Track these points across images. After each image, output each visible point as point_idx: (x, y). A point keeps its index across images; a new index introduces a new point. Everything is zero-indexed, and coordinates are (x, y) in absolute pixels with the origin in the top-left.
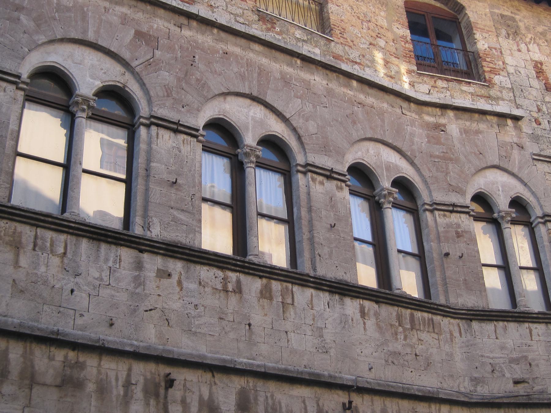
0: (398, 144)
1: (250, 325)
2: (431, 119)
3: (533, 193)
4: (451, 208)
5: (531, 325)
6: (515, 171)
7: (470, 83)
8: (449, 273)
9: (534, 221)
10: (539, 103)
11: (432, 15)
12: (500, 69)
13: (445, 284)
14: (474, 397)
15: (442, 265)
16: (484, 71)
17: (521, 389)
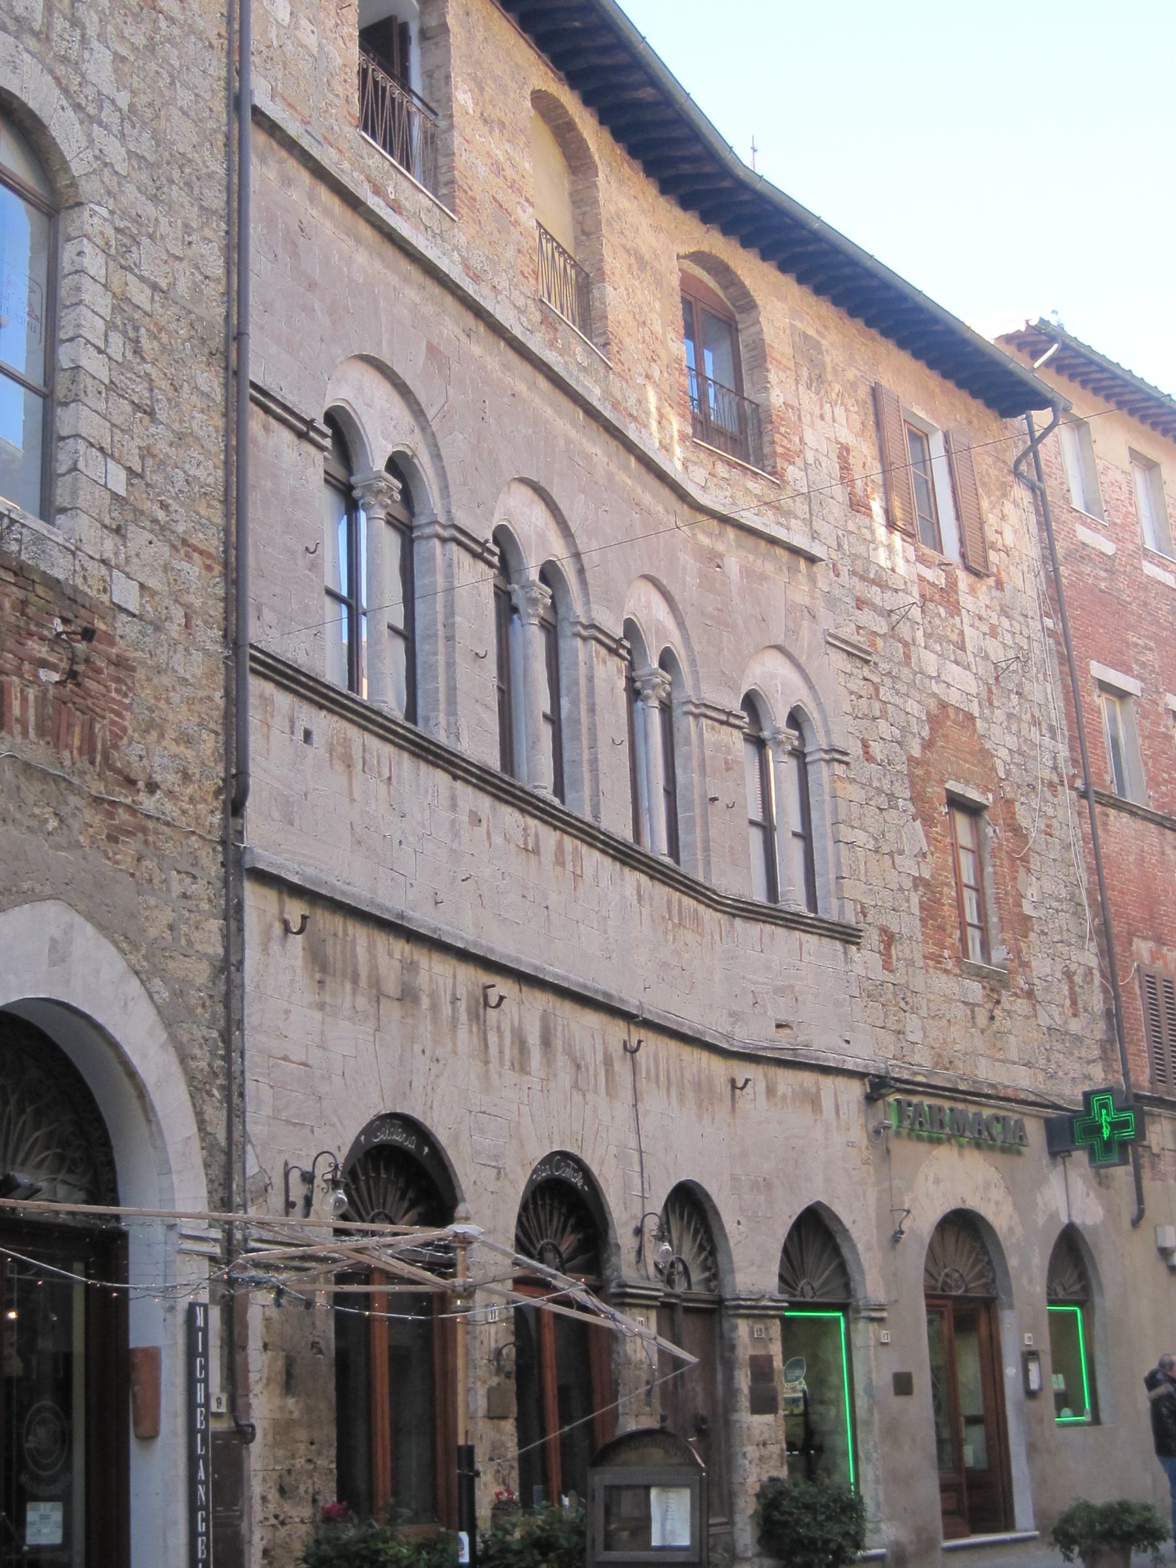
0: (672, 588)
1: (547, 908)
2: (705, 540)
3: (819, 704)
4: (723, 718)
5: (802, 934)
6: (803, 660)
7: (757, 474)
8: (713, 832)
9: (810, 753)
10: (840, 533)
11: (703, 305)
12: (795, 452)
13: (707, 849)
14: (735, 1043)
15: (705, 816)
16: (775, 453)
17: (783, 1039)
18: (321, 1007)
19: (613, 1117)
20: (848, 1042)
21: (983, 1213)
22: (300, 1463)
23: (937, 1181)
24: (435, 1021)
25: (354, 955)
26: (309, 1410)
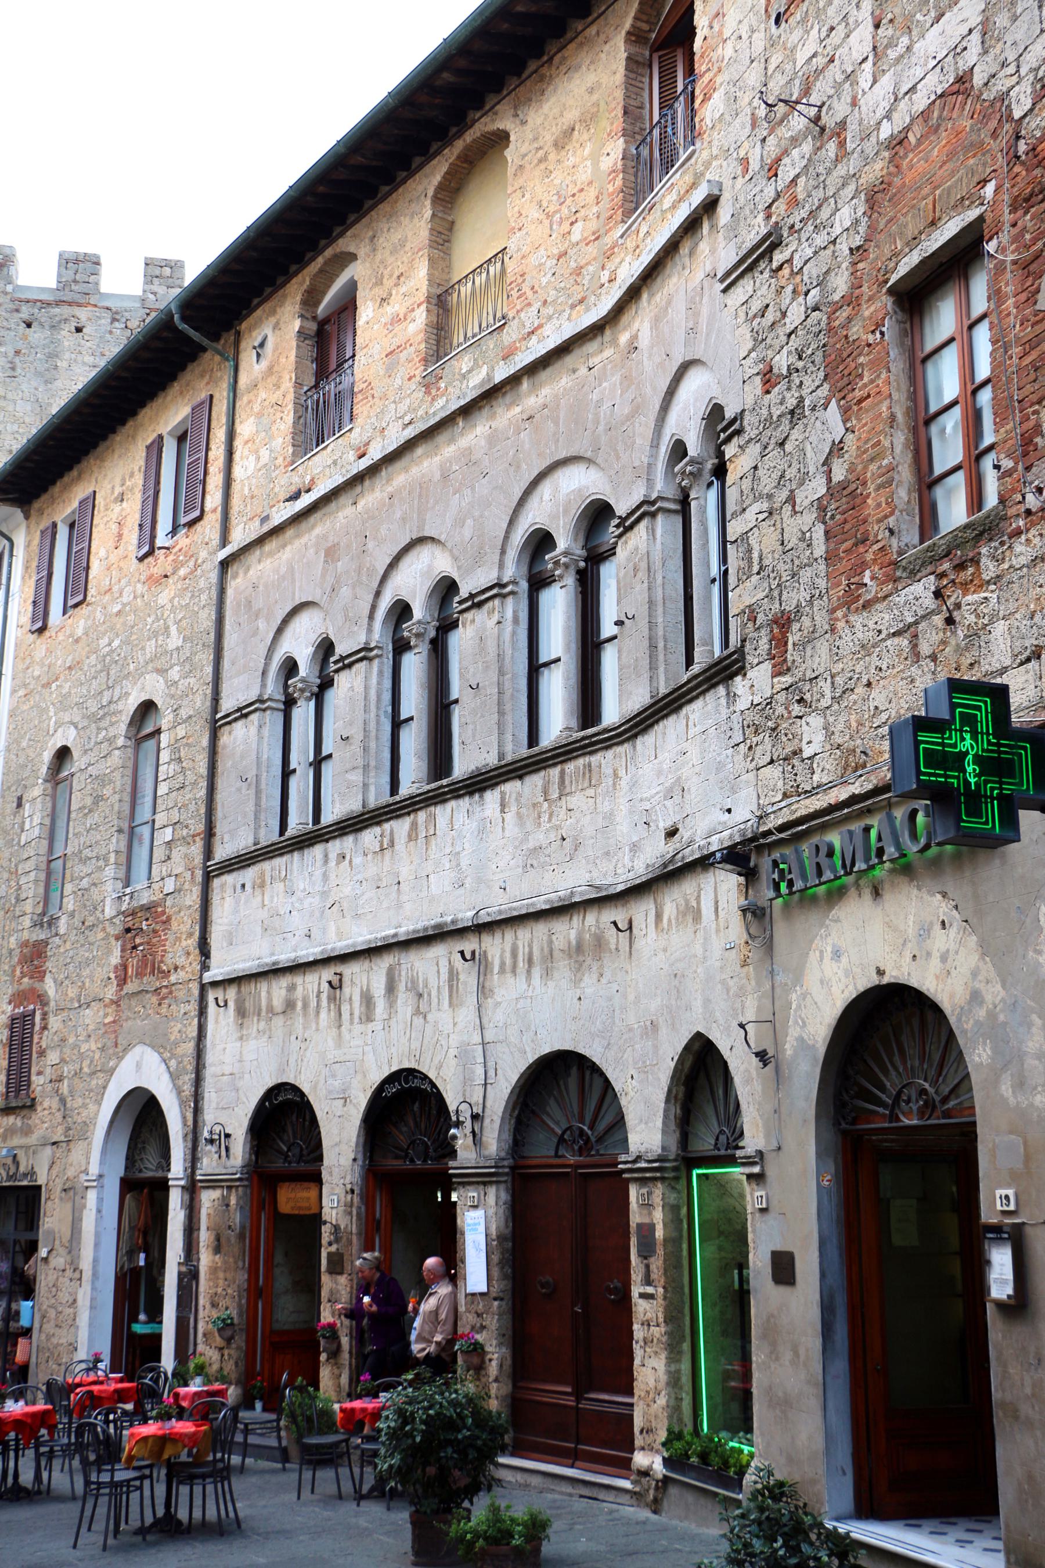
18: (241, 1038)
19: (455, 1024)
20: (729, 811)
21: (914, 983)
22: (220, 1290)
23: (837, 954)
24: (305, 1015)
25: (260, 1000)
26: (225, 1262)
